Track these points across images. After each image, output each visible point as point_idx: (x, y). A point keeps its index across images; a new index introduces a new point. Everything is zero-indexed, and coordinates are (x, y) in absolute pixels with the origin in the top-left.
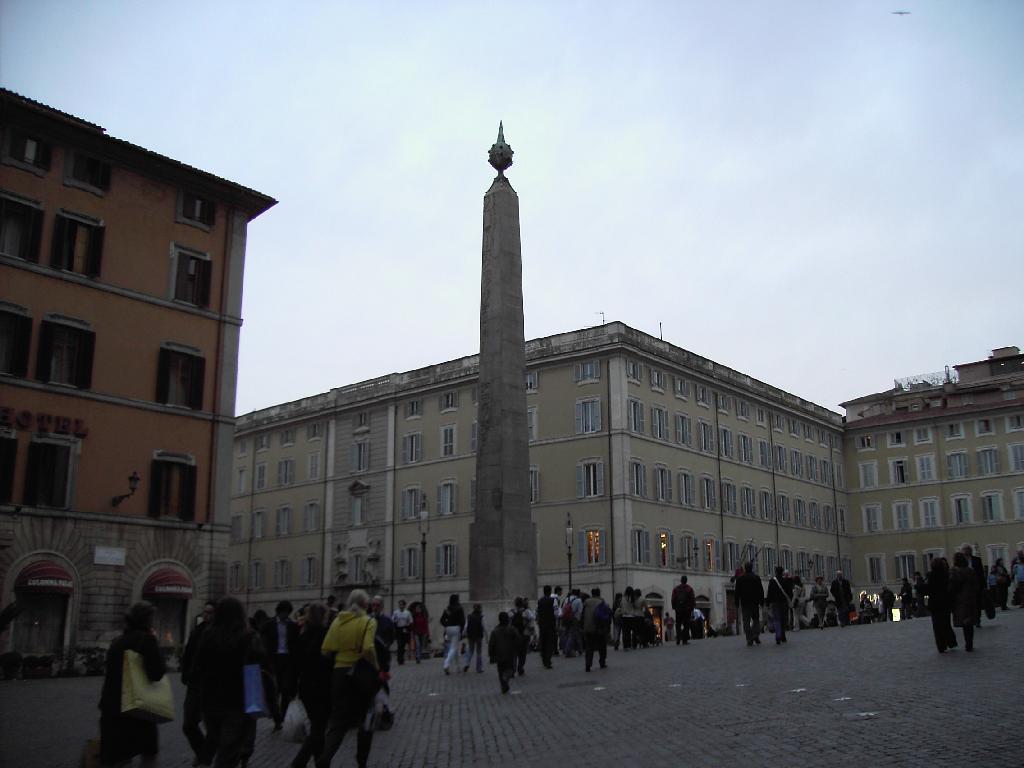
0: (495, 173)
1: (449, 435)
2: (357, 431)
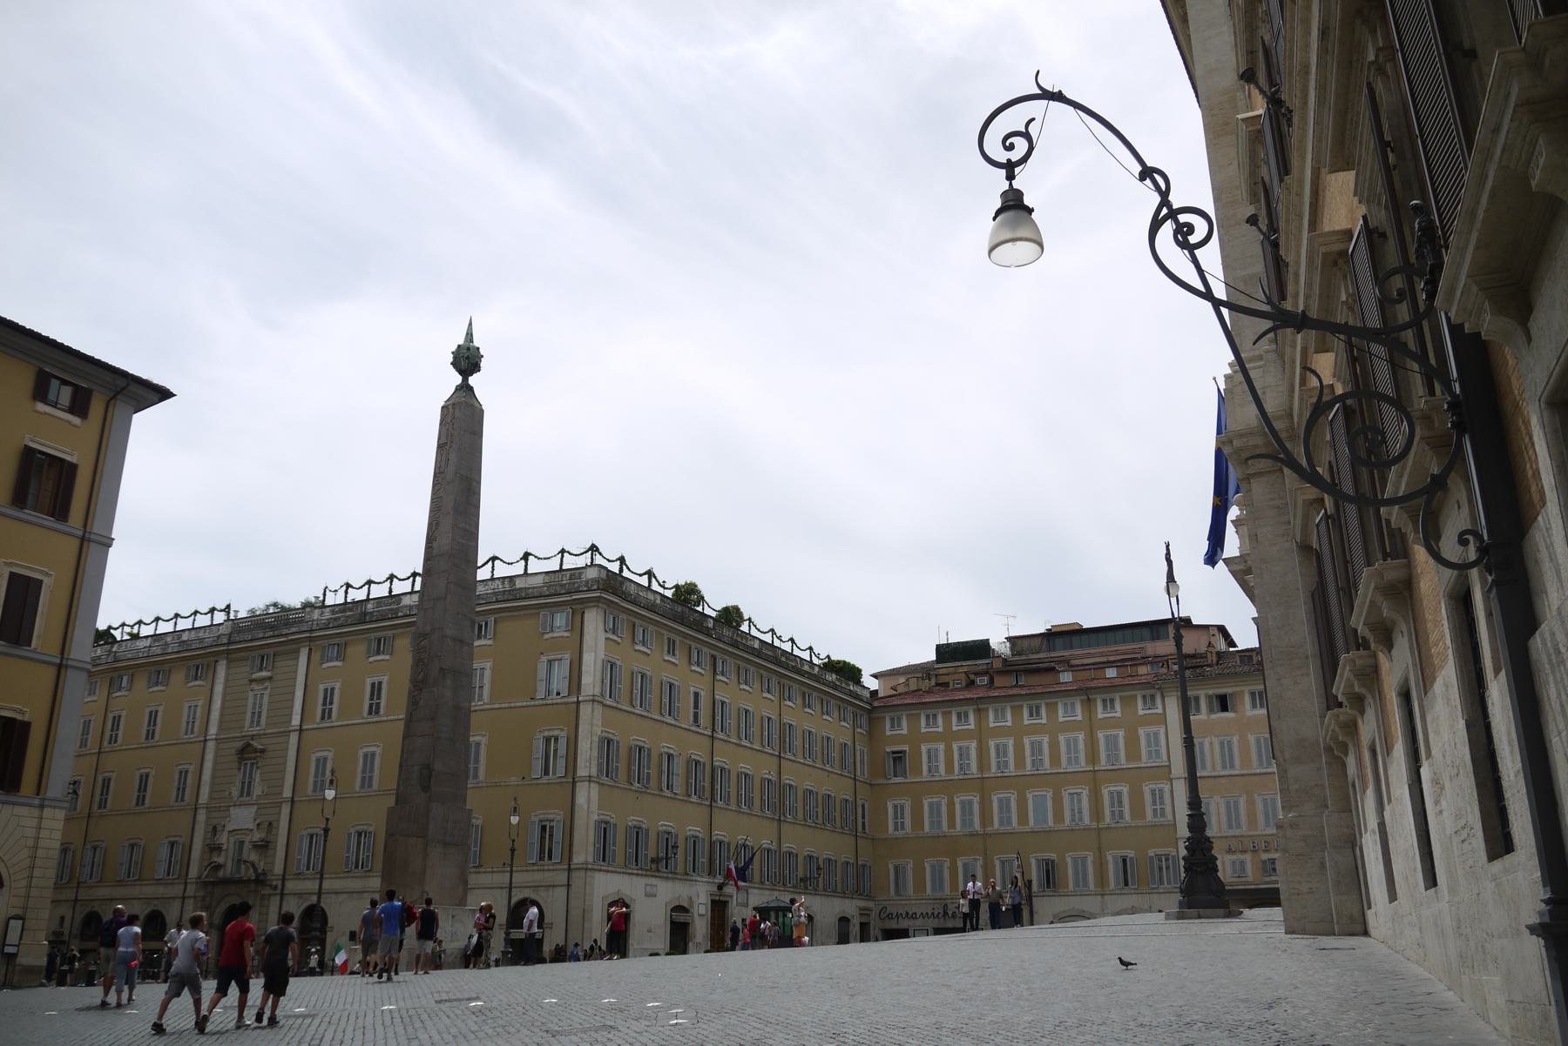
0: (458, 379)
1: (376, 689)
2: (254, 676)
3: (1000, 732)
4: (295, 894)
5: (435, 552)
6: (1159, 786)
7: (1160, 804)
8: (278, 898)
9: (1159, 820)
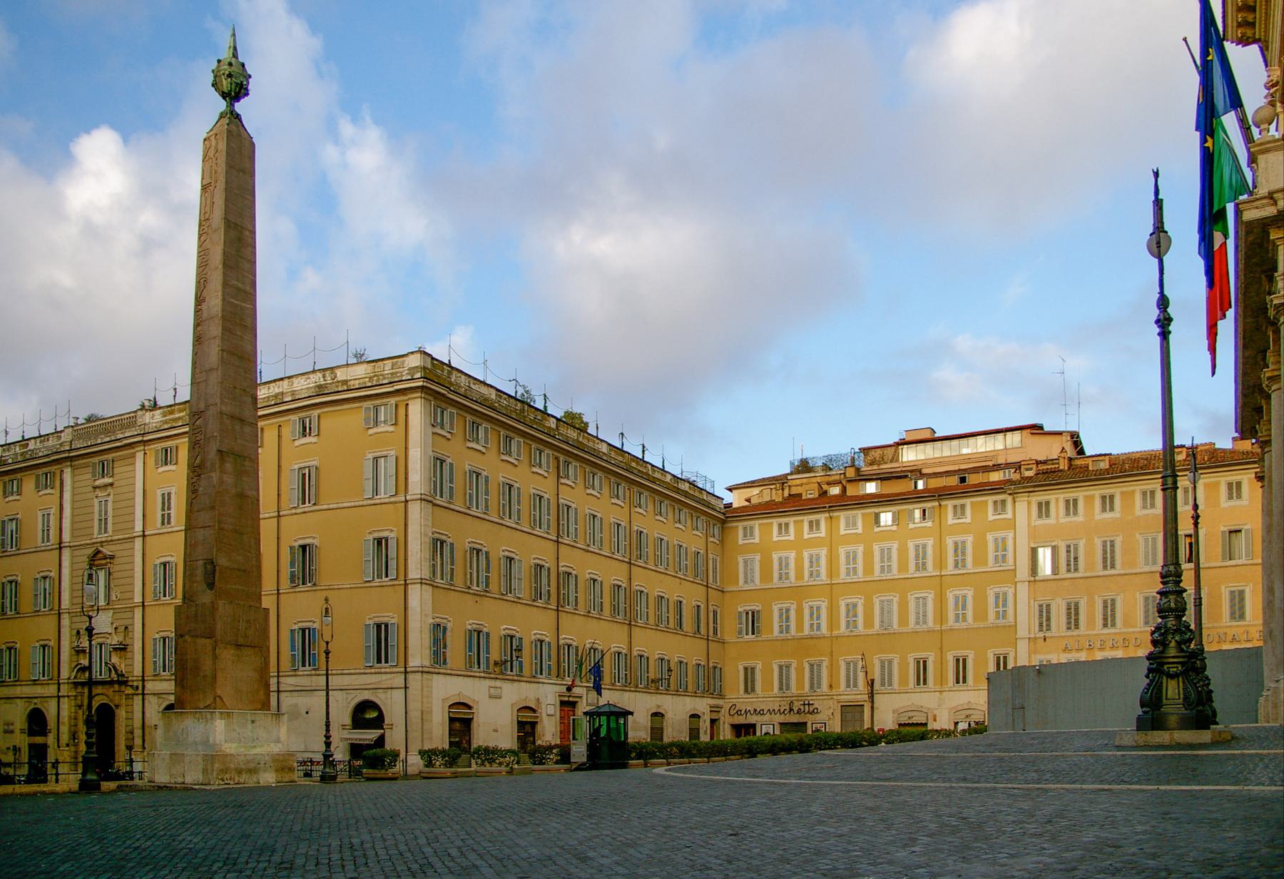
0: (222, 105)
2: (97, 483)
3: (847, 540)
4: (154, 694)
5: (205, 315)
6: (1002, 589)
7: (1003, 606)
8: (141, 697)
9: (1001, 622)
